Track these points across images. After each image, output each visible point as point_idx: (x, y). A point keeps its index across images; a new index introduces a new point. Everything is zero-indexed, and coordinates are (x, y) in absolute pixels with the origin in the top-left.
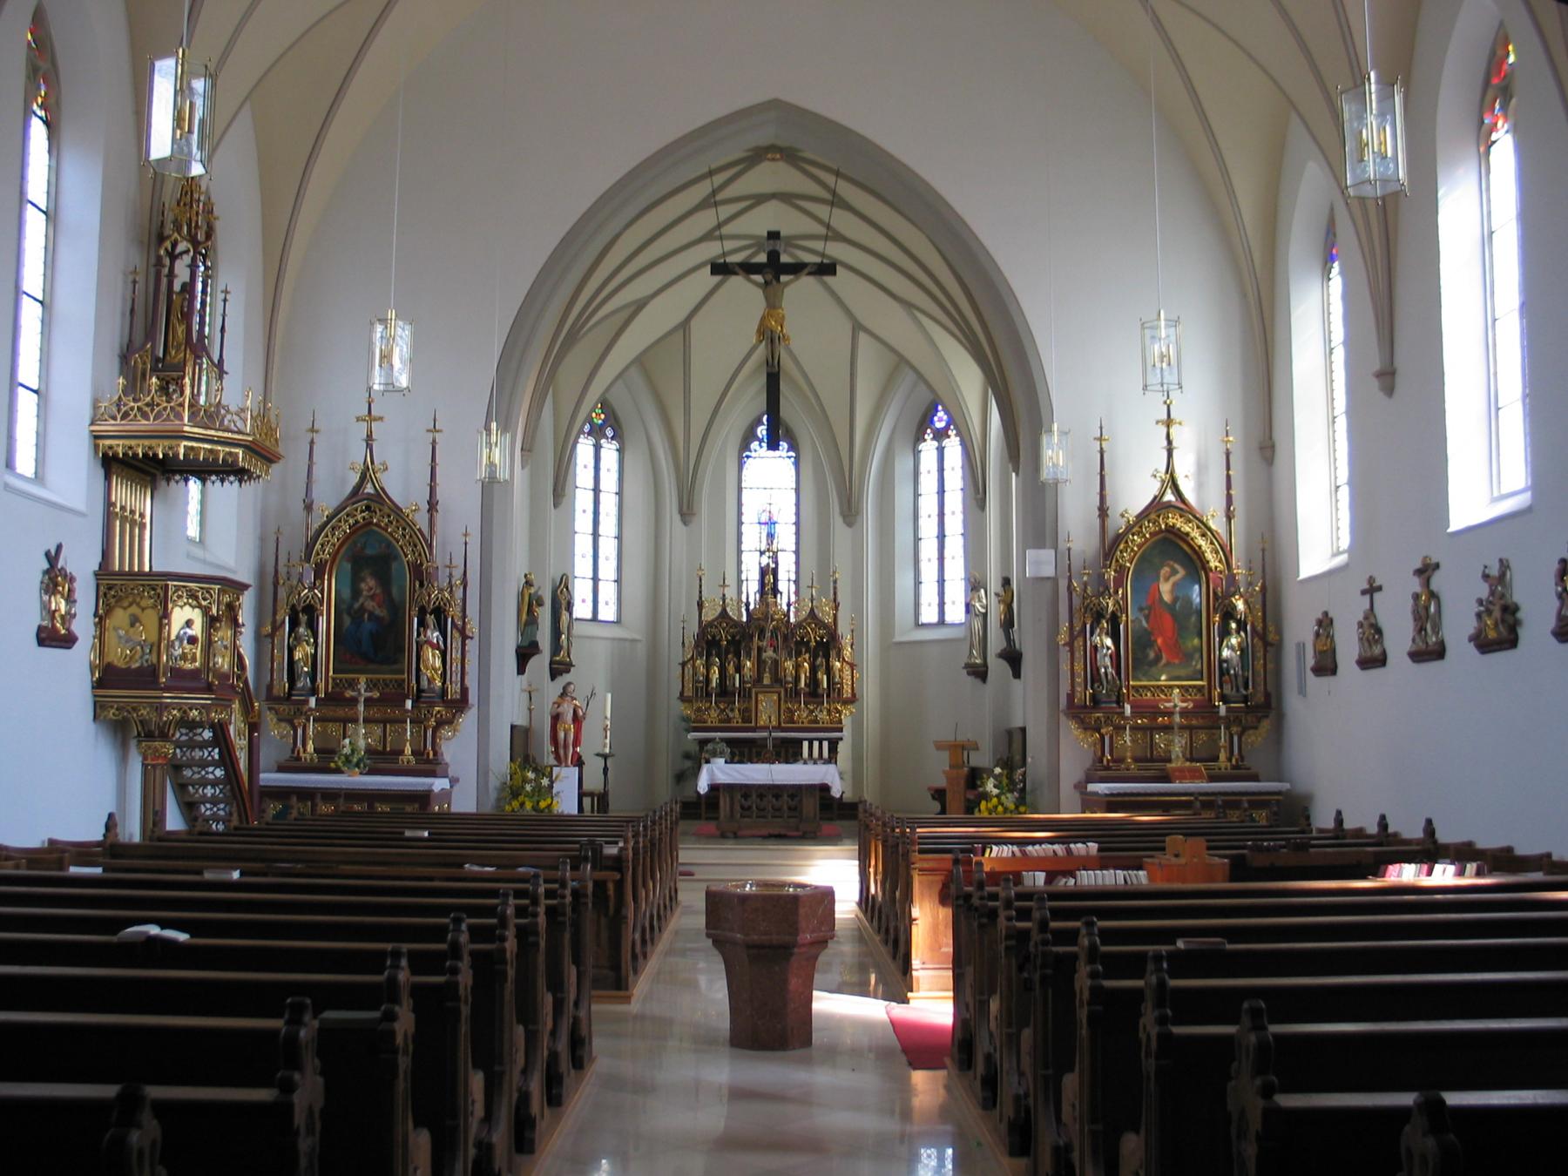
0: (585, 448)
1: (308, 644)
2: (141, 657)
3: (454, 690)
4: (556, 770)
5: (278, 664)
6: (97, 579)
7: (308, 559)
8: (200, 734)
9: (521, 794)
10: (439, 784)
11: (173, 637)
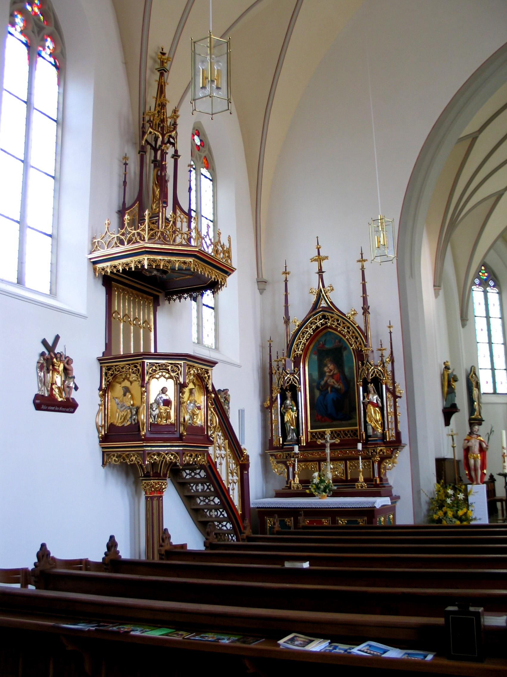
0: (477, 294)
1: (293, 411)
2: (131, 417)
3: (390, 435)
4: (469, 487)
5: (275, 427)
6: (101, 363)
7: (289, 356)
8: (199, 474)
9: (444, 506)
10: (380, 502)
11: (152, 401)
